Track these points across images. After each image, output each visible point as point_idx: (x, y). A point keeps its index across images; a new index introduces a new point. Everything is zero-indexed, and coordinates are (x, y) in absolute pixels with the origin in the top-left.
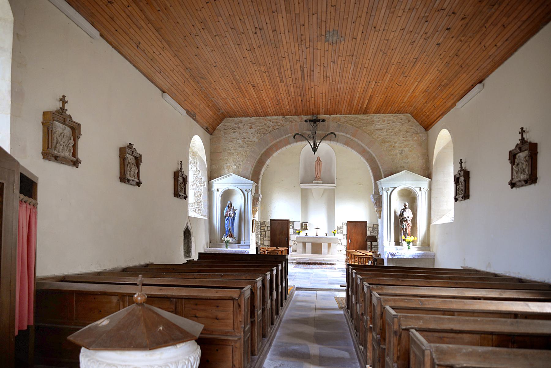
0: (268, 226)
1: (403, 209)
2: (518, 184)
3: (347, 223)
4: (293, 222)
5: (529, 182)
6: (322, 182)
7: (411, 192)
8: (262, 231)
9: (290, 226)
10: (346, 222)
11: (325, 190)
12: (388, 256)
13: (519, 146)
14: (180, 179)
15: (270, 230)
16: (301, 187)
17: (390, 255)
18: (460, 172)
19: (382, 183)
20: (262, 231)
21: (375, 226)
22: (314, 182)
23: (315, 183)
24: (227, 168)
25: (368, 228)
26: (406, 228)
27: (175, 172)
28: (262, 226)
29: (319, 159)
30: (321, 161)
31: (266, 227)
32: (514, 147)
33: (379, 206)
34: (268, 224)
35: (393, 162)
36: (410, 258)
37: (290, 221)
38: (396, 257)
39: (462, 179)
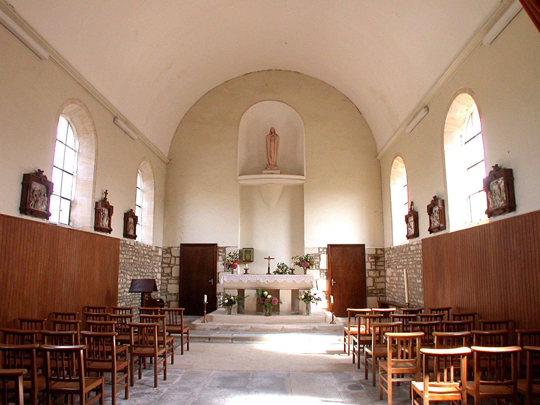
0: (175, 257)
3: (327, 249)
4: (224, 248)
6: (279, 172)
8: (164, 265)
9: (219, 255)
10: (326, 247)
11: (286, 188)
13: (433, 202)
14: (131, 220)
15: (180, 265)
16: (241, 182)
18: (410, 213)
20: (164, 265)
21: (379, 252)
22: (264, 172)
23: (265, 174)
24: (308, 309)
25: (366, 256)
27: (125, 214)
28: (164, 256)
29: (274, 132)
30: (277, 135)
31: (173, 259)
32: (430, 203)
34: (176, 252)
37: (219, 246)
39: (411, 219)
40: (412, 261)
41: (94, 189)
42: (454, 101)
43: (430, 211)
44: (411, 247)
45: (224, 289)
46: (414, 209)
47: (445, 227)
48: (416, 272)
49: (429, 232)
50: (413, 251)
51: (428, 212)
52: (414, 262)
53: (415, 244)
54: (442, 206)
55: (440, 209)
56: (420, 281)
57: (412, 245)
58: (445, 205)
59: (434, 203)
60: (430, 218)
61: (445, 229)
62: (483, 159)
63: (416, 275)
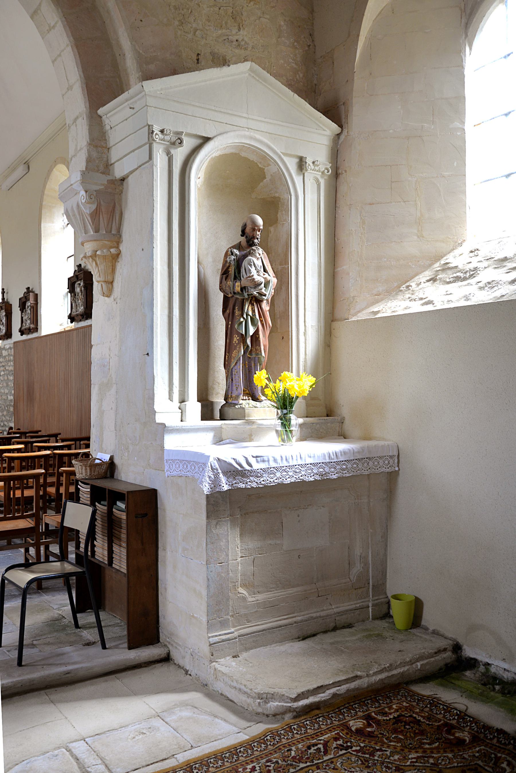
1: (239, 246)
2: (76, 318)
5: (85, 317)
7: (261, 175)
12: (215, 482)
17: (225, 473)
19: (151, 101)
26: (257, 332)
33: (109, 231)
35: (182, 23)
36: (307, 479)
38: (253, 483)
40: (4, 371)
41: (156, 663)
42: (54, 170)
43: (23, 306)
44: (4, 352)
45: (319, 596)
46: (7, 300)
47: (37, 329)
48: (7, 385)
49: (20, 333)
50: (5, 357)
51: (19, 307)
52: (5, 372)
53: (7, 348)
54: (34, 301)
55: (32, 305)
56: (12, 397)
57: (4, 349)
58: (39, 301)
59: (26, 297)
60: (22, 314)
61: (37, 331)
62: (73, 254)
63: (8, 389)
